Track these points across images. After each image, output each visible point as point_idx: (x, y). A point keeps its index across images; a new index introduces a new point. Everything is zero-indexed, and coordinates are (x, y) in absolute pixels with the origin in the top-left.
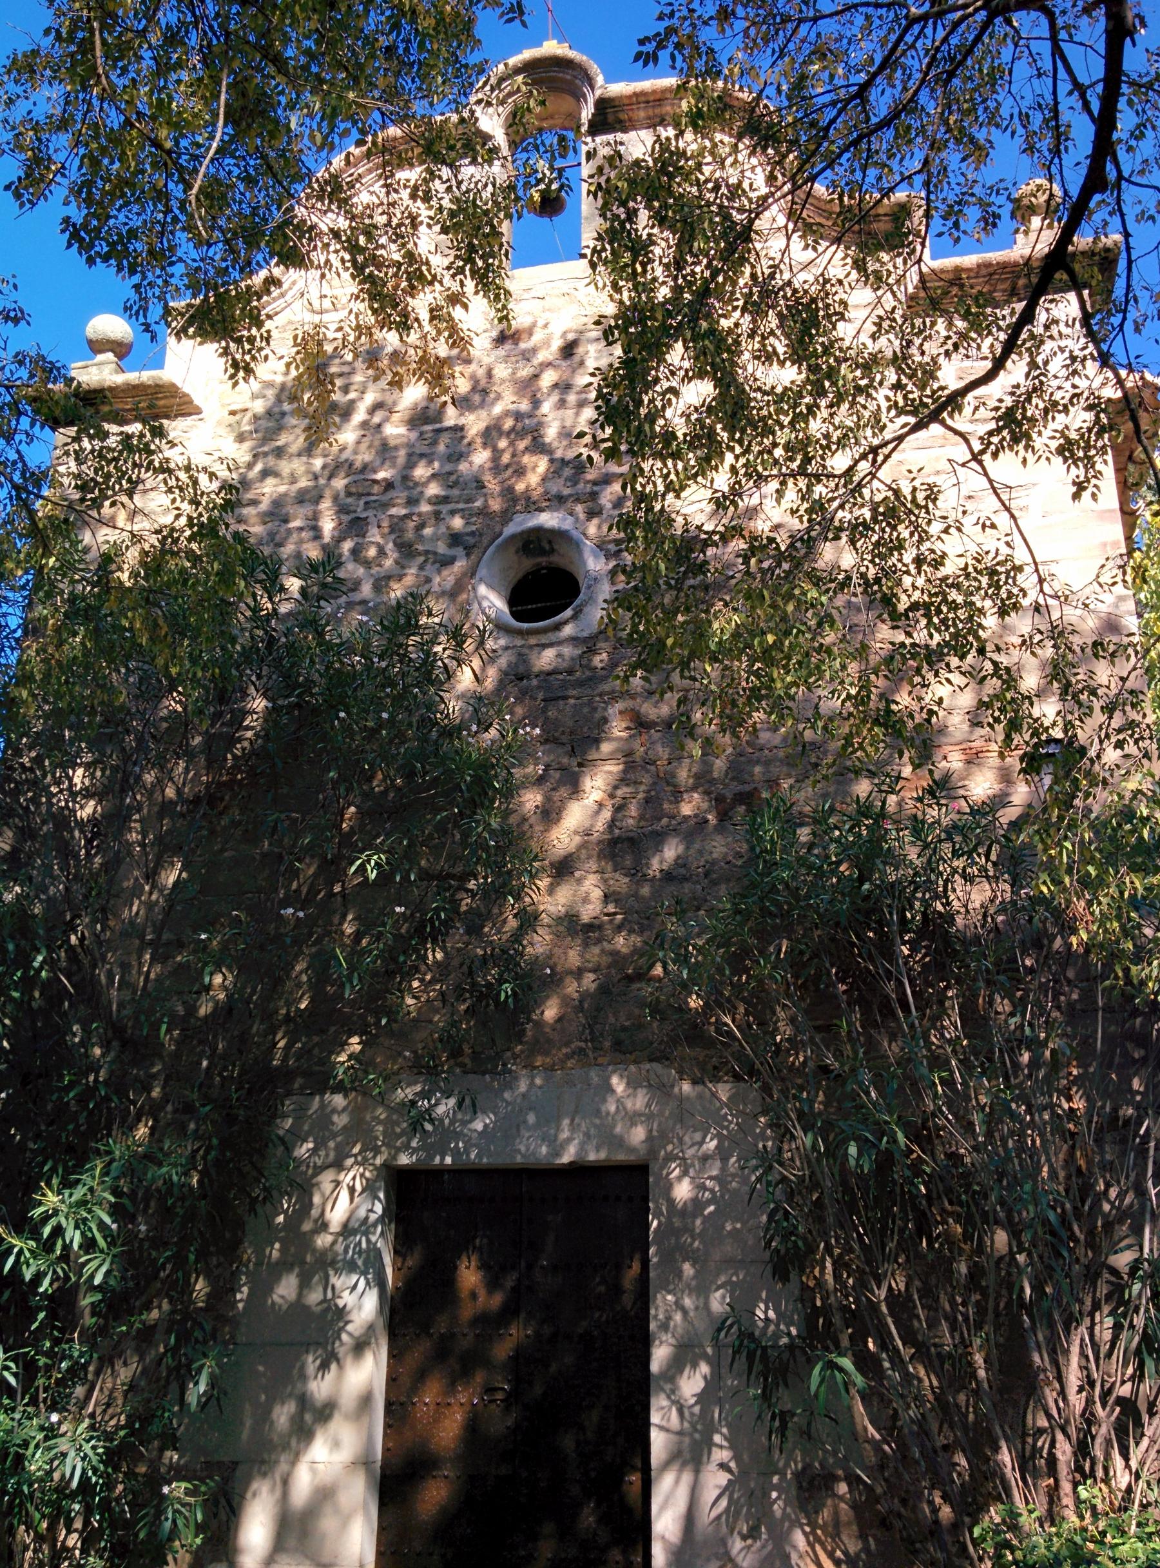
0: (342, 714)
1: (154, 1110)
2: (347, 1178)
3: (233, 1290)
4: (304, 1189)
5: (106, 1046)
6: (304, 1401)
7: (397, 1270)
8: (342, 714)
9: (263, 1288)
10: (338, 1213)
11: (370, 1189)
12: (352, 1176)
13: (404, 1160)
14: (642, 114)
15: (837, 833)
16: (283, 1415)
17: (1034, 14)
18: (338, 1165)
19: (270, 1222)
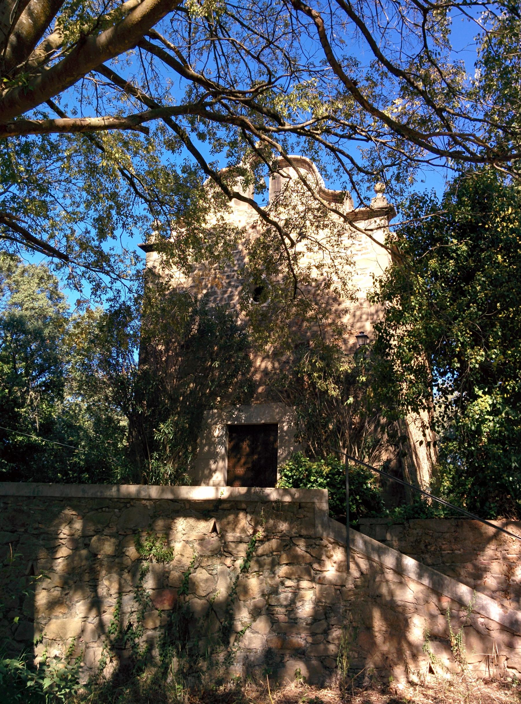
0: (5, 80)
1: (178, 413)
2: (218, 426)
3: (196, 449)
4: (210, 429)
5: (168, 399)
6: (210, 469)
7: (229, 445)
8: (5, 80)
9: (202, 449)
10: (216, 433)
11: (222, 428)
12: (219, 426)
13: (229, 423)
14: (271, 252)
15: (383, 420)
16: (206, 472)
17: (135, 51)
18: (216, 424)
19: (203, 435)
